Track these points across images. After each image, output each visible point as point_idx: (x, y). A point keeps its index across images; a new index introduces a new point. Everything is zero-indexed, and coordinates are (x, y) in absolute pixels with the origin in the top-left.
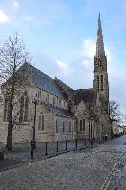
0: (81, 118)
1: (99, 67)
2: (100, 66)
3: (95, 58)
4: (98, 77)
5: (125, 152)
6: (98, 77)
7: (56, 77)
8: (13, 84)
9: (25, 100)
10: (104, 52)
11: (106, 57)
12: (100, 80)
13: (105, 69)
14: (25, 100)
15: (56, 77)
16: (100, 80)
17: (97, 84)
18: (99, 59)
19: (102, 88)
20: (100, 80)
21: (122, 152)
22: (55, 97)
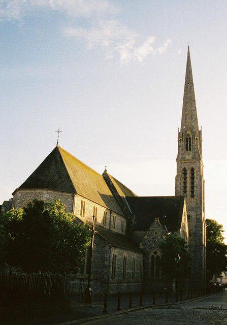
0: (152, 254)
1: (187, 150)
2: (190, 150)
3: (179, 133)
4: (185, 170)
5: (226, 309)
6: (185, 170)
7: (106, 170)
8: (60, 213)
9: (155, 271)
10: (197, 123)
11: (200, 132)
12: (188, 176)
13: (197, 157)
14: (155, 271)
15: (106, 170)
16: (188, 176)
17: (183, 185)
18: (188, 136)
19: (192, 192)
20: (188, 176)
21: (224, 309)
22: (84, 200)
